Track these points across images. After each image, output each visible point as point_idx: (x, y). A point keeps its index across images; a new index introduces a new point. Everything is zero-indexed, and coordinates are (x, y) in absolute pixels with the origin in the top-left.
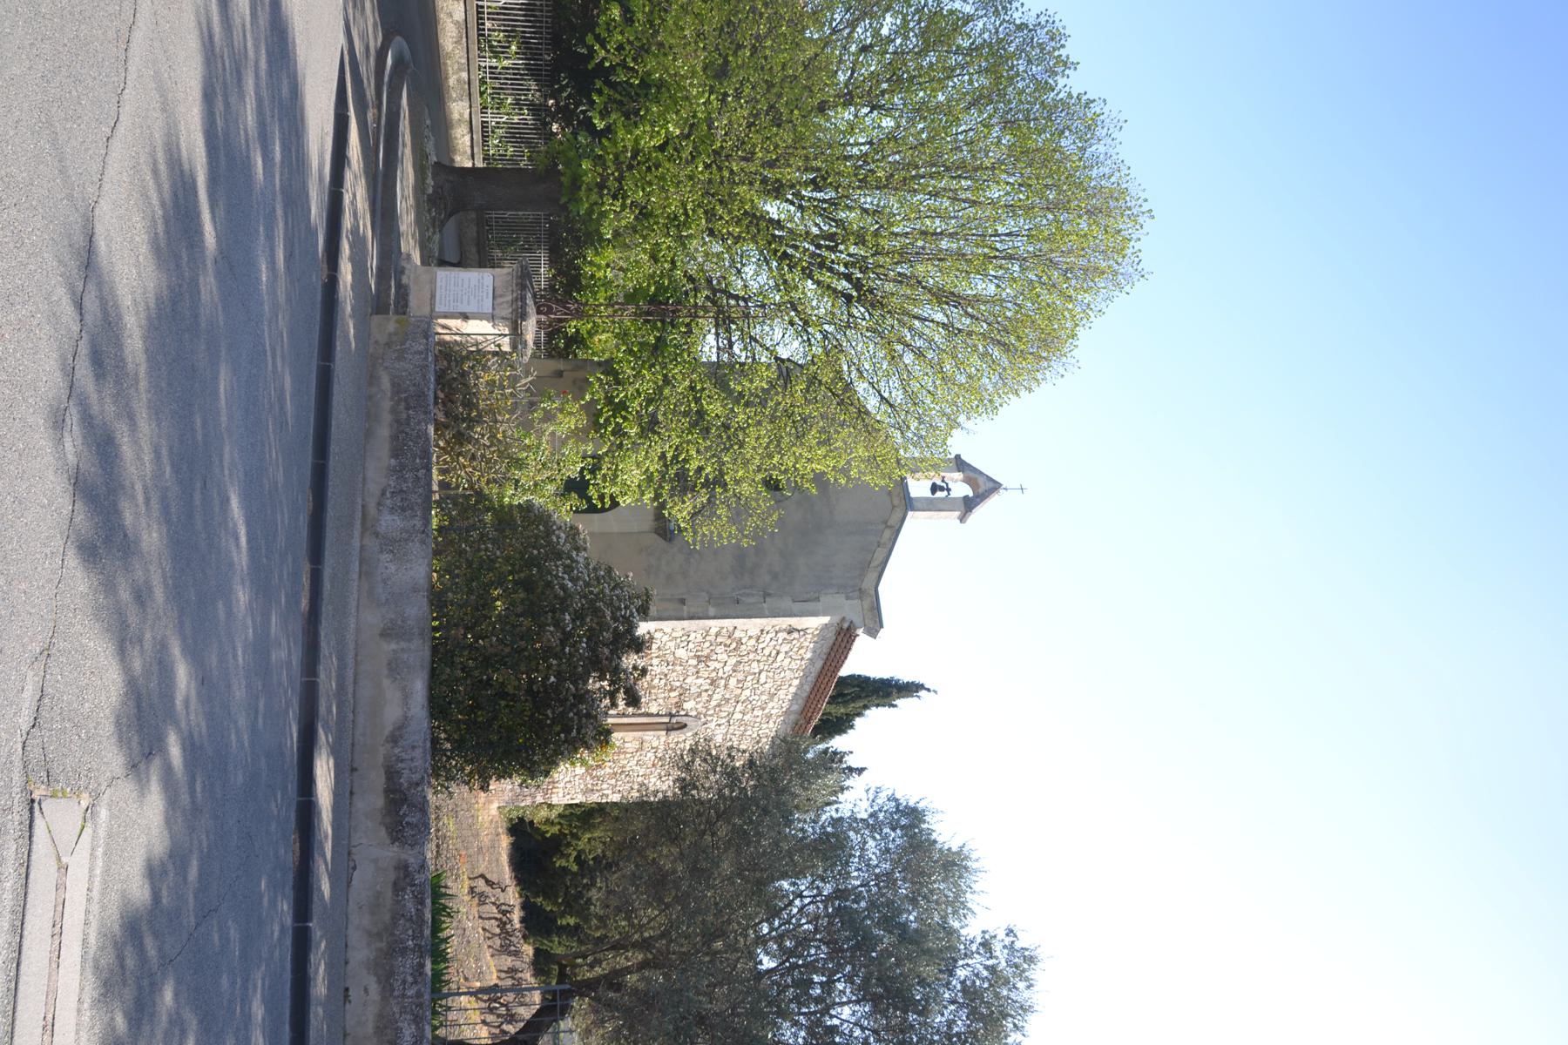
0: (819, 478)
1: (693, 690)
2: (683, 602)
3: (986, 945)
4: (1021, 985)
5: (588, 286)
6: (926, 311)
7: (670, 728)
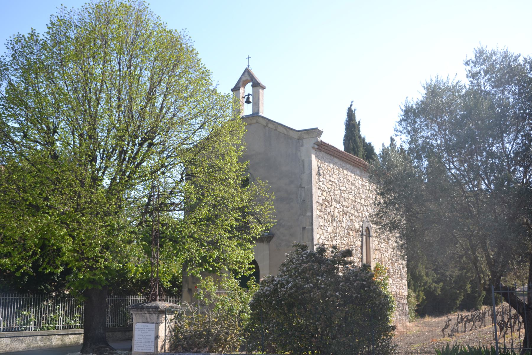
0: (241, 160)
1: (349, 223)
2: (304, 229)
3: (474, 75)
4: (494, 58)
5: (147, 276)
6: (158, 105)
7: (369, 236)
